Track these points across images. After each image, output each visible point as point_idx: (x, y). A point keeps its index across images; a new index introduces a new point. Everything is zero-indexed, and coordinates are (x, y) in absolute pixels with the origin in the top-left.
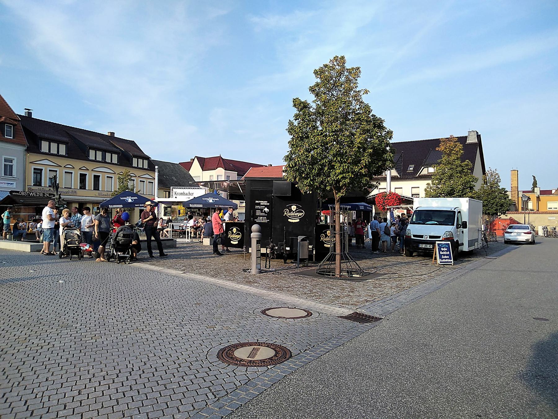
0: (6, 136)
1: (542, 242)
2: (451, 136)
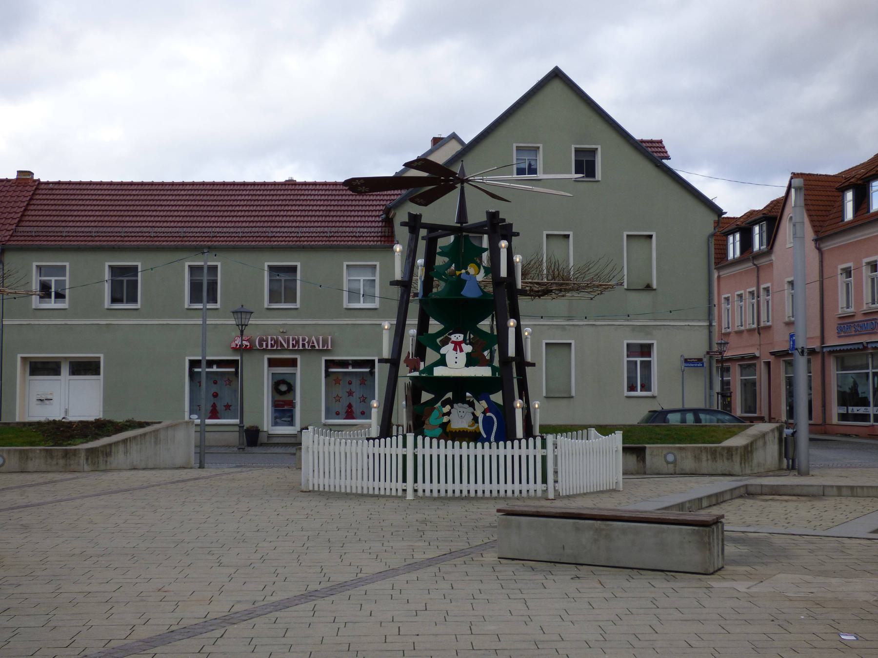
2: (517, 234)
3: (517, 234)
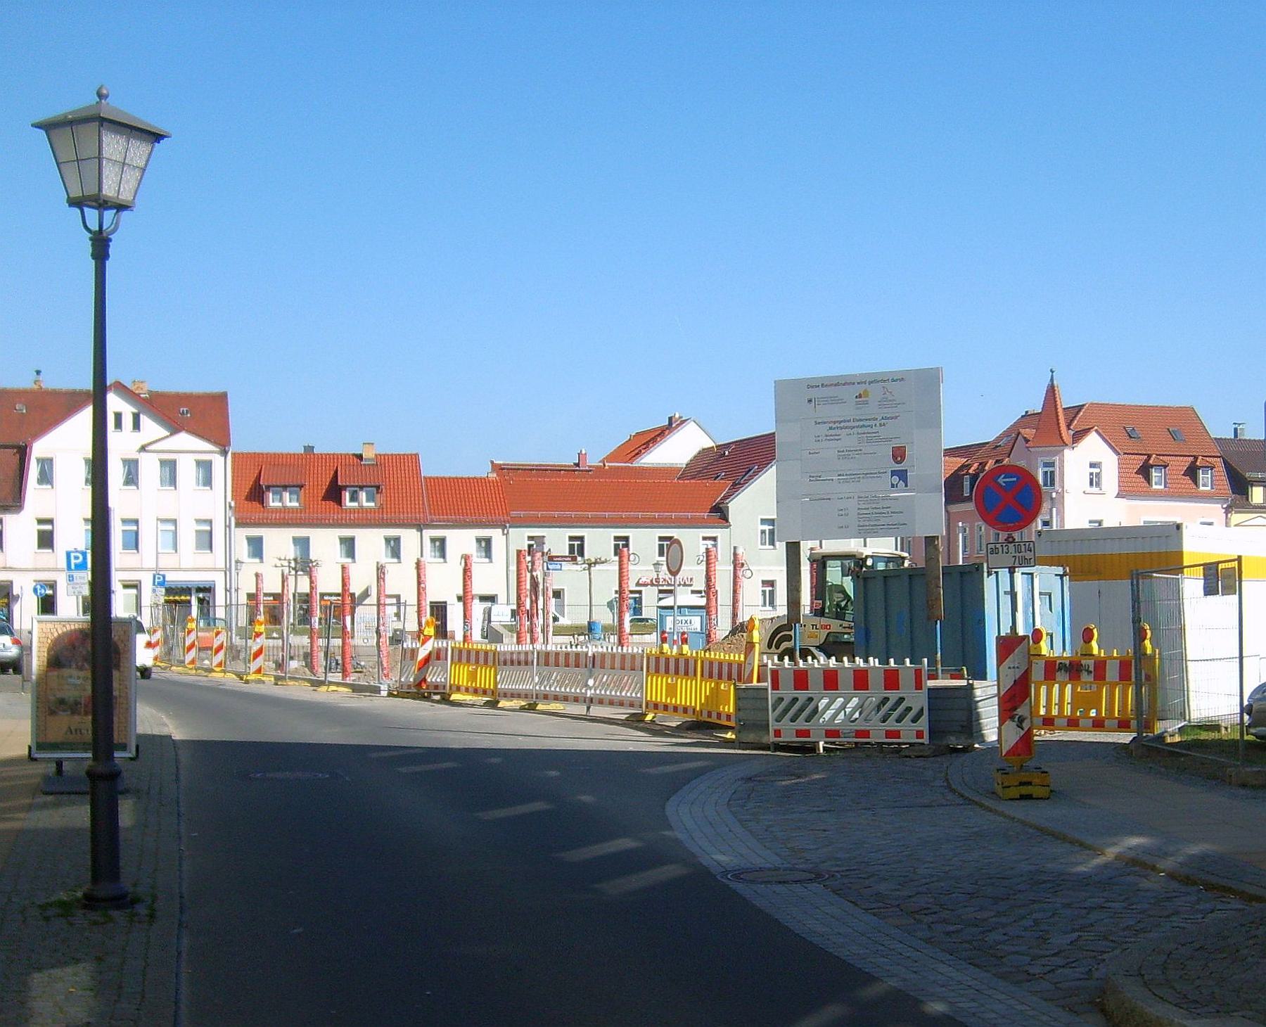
0: (1156, 484)
1: (1048, 382)
3: (86, 520)
